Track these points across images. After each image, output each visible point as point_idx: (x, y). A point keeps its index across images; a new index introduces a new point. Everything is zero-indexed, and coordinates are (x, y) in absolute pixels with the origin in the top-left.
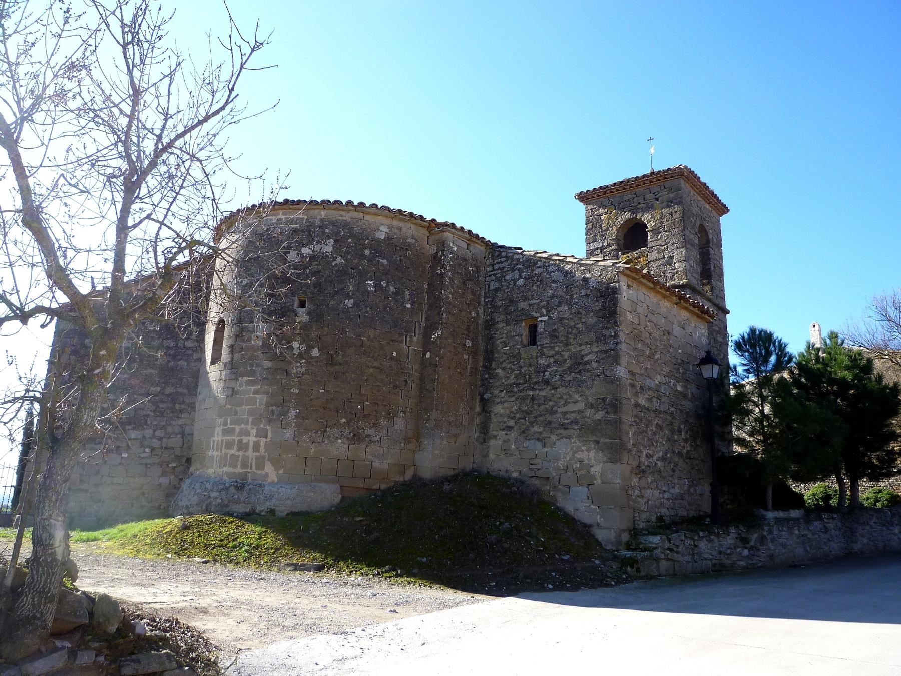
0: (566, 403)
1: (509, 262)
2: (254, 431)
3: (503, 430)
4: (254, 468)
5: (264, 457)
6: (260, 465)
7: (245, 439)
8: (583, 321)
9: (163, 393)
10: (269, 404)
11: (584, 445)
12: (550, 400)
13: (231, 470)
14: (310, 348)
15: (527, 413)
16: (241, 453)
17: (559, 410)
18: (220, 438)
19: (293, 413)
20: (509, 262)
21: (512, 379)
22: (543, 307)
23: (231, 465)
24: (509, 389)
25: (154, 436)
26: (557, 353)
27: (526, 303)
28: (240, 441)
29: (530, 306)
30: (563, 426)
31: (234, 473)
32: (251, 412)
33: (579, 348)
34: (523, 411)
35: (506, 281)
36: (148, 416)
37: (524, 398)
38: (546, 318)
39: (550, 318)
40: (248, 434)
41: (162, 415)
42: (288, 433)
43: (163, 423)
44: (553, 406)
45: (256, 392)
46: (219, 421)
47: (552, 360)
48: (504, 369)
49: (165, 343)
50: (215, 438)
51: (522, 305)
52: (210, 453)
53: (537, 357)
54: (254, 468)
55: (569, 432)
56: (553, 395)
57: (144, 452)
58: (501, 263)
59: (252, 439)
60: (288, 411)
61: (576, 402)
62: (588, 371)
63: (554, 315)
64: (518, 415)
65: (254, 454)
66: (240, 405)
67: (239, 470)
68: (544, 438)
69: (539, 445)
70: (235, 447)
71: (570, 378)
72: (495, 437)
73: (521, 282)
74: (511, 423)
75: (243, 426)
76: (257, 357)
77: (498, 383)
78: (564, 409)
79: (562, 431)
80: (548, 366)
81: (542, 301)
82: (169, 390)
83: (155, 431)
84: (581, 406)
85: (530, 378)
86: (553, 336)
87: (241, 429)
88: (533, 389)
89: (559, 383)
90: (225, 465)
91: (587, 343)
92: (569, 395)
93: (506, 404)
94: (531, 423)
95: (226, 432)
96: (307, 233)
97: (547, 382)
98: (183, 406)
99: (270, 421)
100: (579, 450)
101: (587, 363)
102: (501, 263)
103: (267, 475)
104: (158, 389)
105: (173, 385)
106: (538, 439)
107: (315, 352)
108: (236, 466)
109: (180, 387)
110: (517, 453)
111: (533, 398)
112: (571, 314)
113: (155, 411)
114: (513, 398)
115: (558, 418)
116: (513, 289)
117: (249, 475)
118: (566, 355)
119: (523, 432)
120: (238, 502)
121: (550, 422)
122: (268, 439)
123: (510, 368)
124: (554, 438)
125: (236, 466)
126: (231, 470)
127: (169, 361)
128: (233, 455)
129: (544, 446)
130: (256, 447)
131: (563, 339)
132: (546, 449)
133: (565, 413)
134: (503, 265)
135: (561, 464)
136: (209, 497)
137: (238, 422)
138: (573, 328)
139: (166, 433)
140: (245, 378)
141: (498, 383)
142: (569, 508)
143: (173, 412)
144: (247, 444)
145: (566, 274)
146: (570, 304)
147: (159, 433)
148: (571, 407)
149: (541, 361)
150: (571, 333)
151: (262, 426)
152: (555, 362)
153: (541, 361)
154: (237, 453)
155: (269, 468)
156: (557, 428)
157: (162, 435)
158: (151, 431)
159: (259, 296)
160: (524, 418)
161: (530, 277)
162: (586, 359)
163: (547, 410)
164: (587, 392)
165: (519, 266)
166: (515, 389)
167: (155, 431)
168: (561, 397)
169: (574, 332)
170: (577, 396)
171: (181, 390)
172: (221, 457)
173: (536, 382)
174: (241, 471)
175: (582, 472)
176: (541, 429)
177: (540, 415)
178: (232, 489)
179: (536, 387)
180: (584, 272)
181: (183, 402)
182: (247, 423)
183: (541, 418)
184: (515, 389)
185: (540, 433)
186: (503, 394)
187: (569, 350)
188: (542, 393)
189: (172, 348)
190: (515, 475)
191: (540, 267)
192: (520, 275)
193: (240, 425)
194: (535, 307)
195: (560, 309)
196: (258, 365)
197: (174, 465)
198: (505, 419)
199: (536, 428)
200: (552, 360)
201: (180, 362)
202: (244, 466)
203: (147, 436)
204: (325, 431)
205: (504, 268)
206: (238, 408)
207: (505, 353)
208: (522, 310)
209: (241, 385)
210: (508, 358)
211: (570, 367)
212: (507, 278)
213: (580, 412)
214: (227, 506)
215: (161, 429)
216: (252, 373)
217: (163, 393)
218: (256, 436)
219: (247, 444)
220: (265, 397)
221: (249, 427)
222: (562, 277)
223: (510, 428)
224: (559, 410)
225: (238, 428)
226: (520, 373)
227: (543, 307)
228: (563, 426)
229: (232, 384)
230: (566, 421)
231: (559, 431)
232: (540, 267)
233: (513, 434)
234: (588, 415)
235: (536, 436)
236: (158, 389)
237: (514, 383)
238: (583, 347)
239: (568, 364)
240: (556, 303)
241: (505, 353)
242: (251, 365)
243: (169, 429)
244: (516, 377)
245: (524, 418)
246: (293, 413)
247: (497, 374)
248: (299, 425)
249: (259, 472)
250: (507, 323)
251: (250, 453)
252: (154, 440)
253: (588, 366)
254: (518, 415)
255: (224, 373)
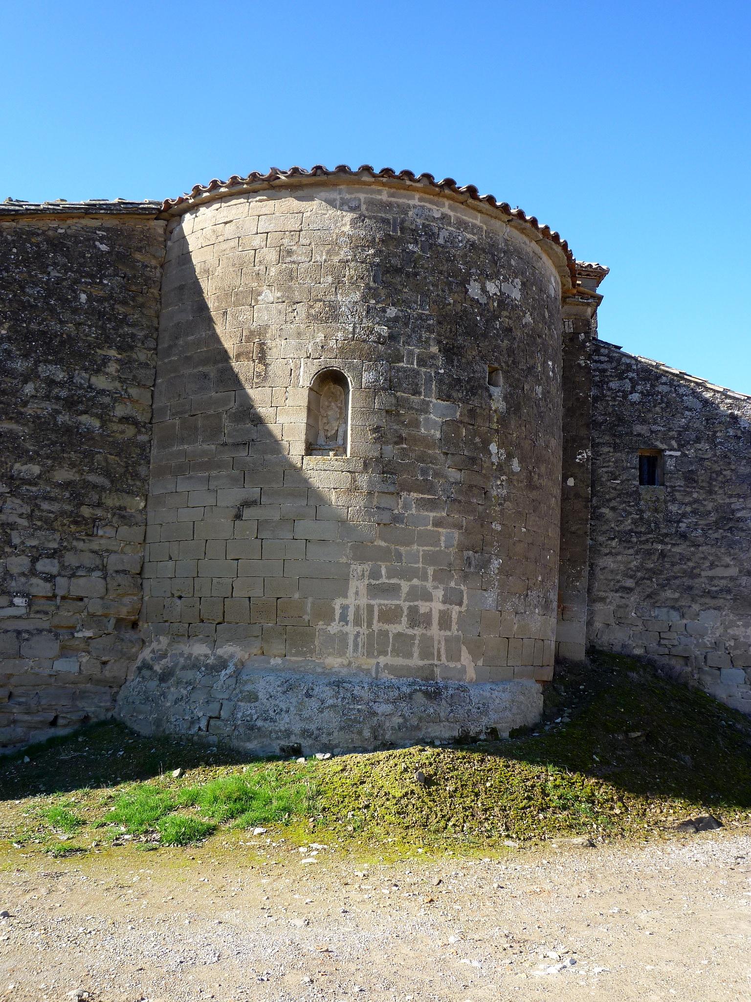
0: (712, 566)
1: (614, 364)
2: (439, 594)
3: (617, 591)
4: (443, 657)
5: (457, 638)
6: (454, 656)
7: (423, 607)
8: (733, 467)
9: (48, 481)
10: (462, 548)
11: (739, 620)
12: (689, 560)
13: (399, 661)
14: (510, 456)
15: (653, 571)
16: (417, 631)
17: (703, 574)
18: (363, 601)
19: (496, 563)
20: (614, 364)
21: (627, 525)
22: (673, 438)
23: (396, 652)
24: (624, 538)
25: (33, 572)
26: (696, 501)
27: (645, 427)
28: (413, 610)
29: (652, 432)
30: (708, 594)
31: (408, 668)
32: (430, 559)
33: (727, 501)
34: (647, 570)
35: (610, 389)
36: (13, 526)
37: (649, 553)
38: (678, 454)
39: (684, 455)
40: (428, 597)
41: (49, 525)
42: (491, 598)
43: (55, 545)
44: (694, 568)
45: (438, 523)
46: (357, 568)
47: (689, 509)
48: (613, 509)
49: (44, 370)
50: (351, 601)
51: (638, 428)
52: (334, 628)
53: (666, 502)
54: (443, 657)
55: (720, 602)
56: (693, 554)
57: (12, 604)
58: (602, 363)
59: (437, 606)
60: (489, 561)
61: (727, 566)
62: (743, 531)
63: (691, 453)
64: (639, 574)
65: (442, 633)
66: (409, 543)
67: (416, 661)
68: (681, 607)
69: (675, 615)
70: (404, 619)
71: (716, 535)
72: (602, 600)
73: (635, 397)
74: (630, 583)
75: (415, 581)
76: (433, 460)
77: (605, 528)
78: (710, 573)
79: (707, 600)
80: (684, 515)
81: (670, 429)
82: (62, 475)
83: (34, 560)
84: (733, 571)
85: (657, 526)
86: (690, 478)
87: (413, 588)
88: (662, 542)
89: (701, 540)
90: (384, 653)
91: (739, 496)
92: (716, 555)
93: (619, 558)
94: (663, 587)
95: (375, 591)
96: (491, 258)
97: (684, 536)
98: (99, 512)
99: (465, 577)
100: (732, 624)
101: (739, 520)
102: (602, 363)
103: (464, 670)
104: (36, 469)
105: (73, 465)
106: (673, 608)
107: (516, 466)
108: (409, 655)
109: (91, 471)
110: (640, 623)
111: (663, 555)
112: (715, 455)
113: (30, 517)
114: (631, 551)
115: (701, 583)
116: (622, 404)
117: (437, 671)
118: (710, 506)
119: (649, 596)
120: (437, 720)
121: (690, 588)
122: (463, 609)
123: (625, 510)
124: (696, 607)
125: (409, 655)
126: (399, 661)
127: (58, 412)
128: (399, 635)
129: (683, 616)
130: (445, 621)
131: (704, 484)
132: (685, 621)
133: (712, 578)
134: (604, 366)
135: (708, 640)
136: (375, 714)
137: (407, 574)
138: (719, 473)
139: (63, 567)
140: (414, 495)
141: (605, 528)
142: (722, 694)
143: (76, 523)
144: (428, 616)
145: (706, 402)
146: (712, 440)
147: (45, 566)
148: (719, 572)
149: (674, 508)
150: (716, 480)
151: (452, 584)
152: (694, 512)
153: (674, 508)
154: (410, 632)
155: (466, 658)
156: (701, 596)
157: (55, 570)
158: (25, 561)
159: (421, 353)
160: (650, 579)
161: (649, 394)
162: (739, 515)
163: (685, 572)
164: (742, 556)
165: (631, 375)
166: (634, 540)
167: (34, 560)
168: (705, 558)
169: (720, 479)
170: (727, 560)
171: (92, 478)
172: (370, 636)
173: (666, 535)
174: (421, 663)
175: (738, 652)
176: (677, 595)
177: (676, 578)
178: (420, 698)
179: (667, 540)
180: (731, 407)
181: (99, 505)
182: (424, 578)
183: (677, 582)
184: (634, 540)
185: (677, 600)
186: (614, 543)
187: (714, 500)
188: (676, 549)
189: (61, 384)
190: (638, 651)
191: (665, 384)
192: (633, 387)
193: (410, 580)
194: (660, 435)
195: (699, 446)
196: (436, 474)
197: (89, 634)
198: (618, 577)
199: (669, 594)
200: (689, 509)
201: (84, 418)
202: (426, 653)
203: (15, 570)
204: (527, 595)
205: (605, 370)
206: (402, 549)
207: (615, 489)
208: (639, 435)
209: (406, 507)
210: (619, 496)
211: (716, 522)
212: (612, 385)
213: (732, 579)
214: (418, 728)
215: (51, 556)
216: (428, 487)
217: (48, 481)
218: (444, 602)
219: (428, 616)
220: (456, 534)
221: (429, 585)
222: (699, 405)
223: (629, 590)
224: (703, 574)
225: (405, 586)
226: (642, 518)
227: (673, 438)
228: (708, 594)
229: (387, 501)
230: (714, 589)
231: (703, 600)
232: (665, 384)
233: (633, 598)
234: (744, 584)
235: (669, 603)
236: (36, 469)
237: (631, 531)
238: (733, 500)
239: (713, 517)
240: (693, 437)
241: (615, 489)
242: (424, 472)
243: (71, 559)
244: (634, 522)
245: (650, 579)
246: (496, 563)
247: (602, 515)
248: (502, 586)
249: (452, 665)
250: (616, 447)
251: (435, 630)
252: (35, 580)
253: (741, 525)
254: (639, 574)
255: (363, 480)
